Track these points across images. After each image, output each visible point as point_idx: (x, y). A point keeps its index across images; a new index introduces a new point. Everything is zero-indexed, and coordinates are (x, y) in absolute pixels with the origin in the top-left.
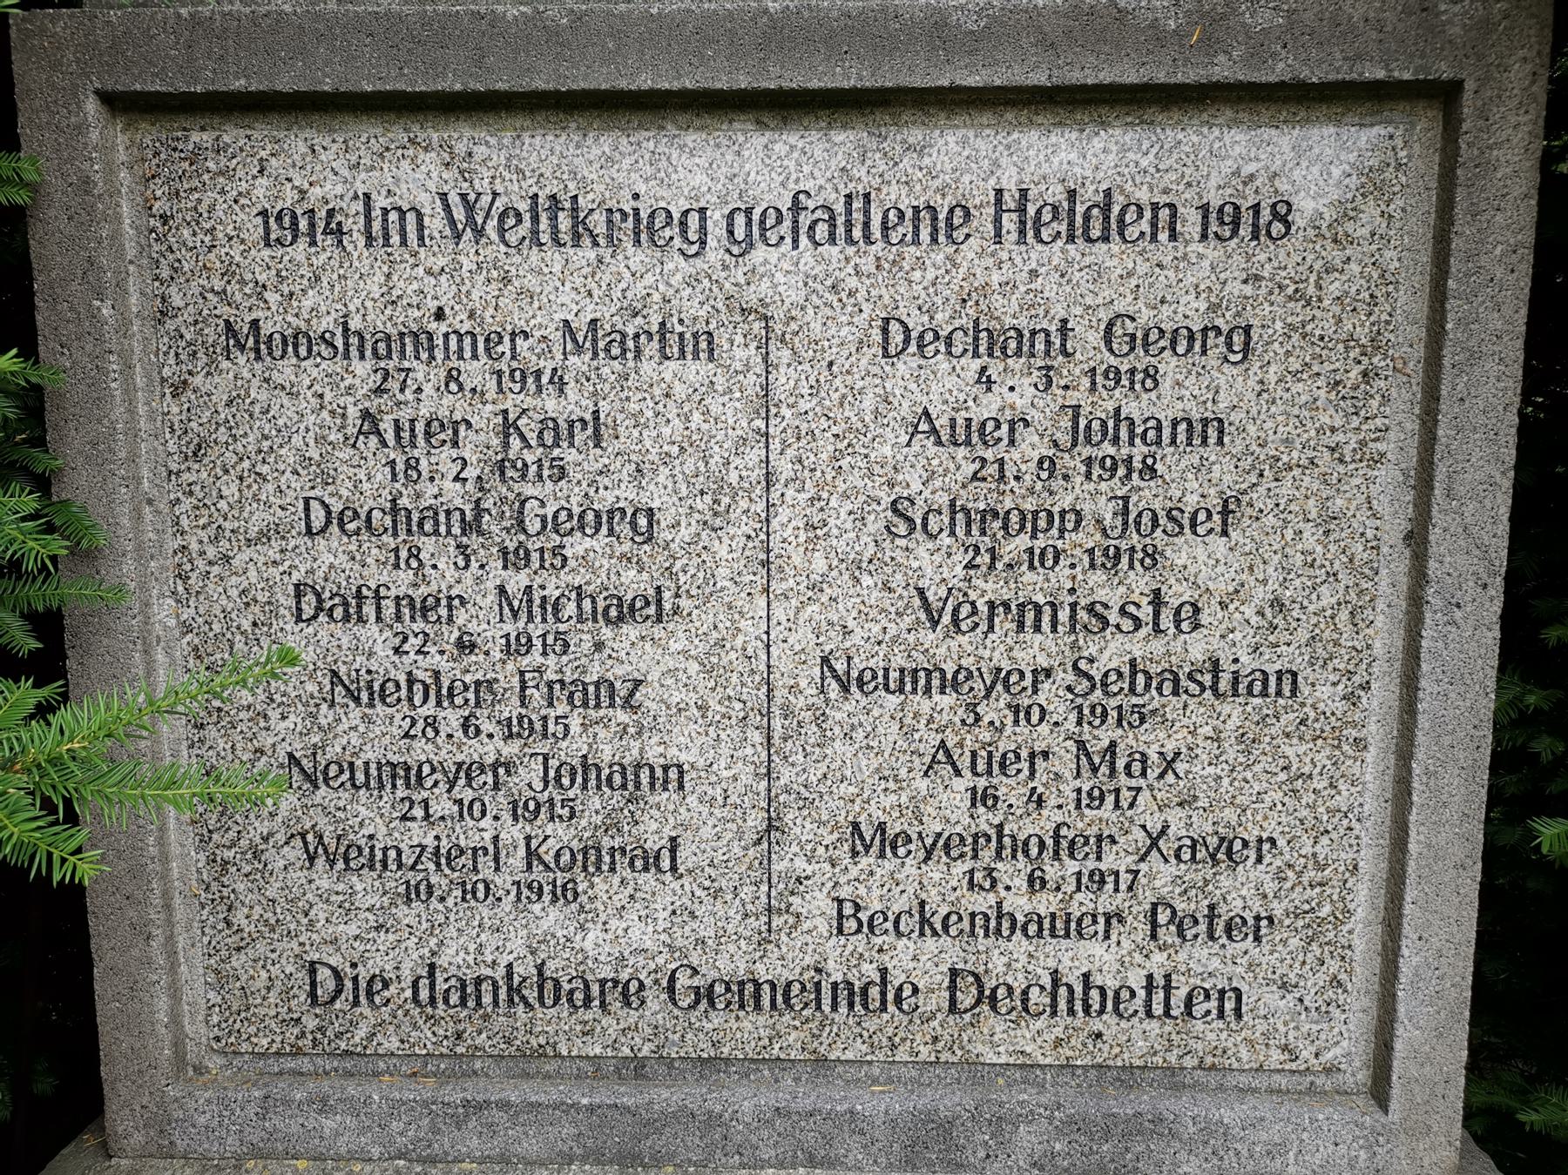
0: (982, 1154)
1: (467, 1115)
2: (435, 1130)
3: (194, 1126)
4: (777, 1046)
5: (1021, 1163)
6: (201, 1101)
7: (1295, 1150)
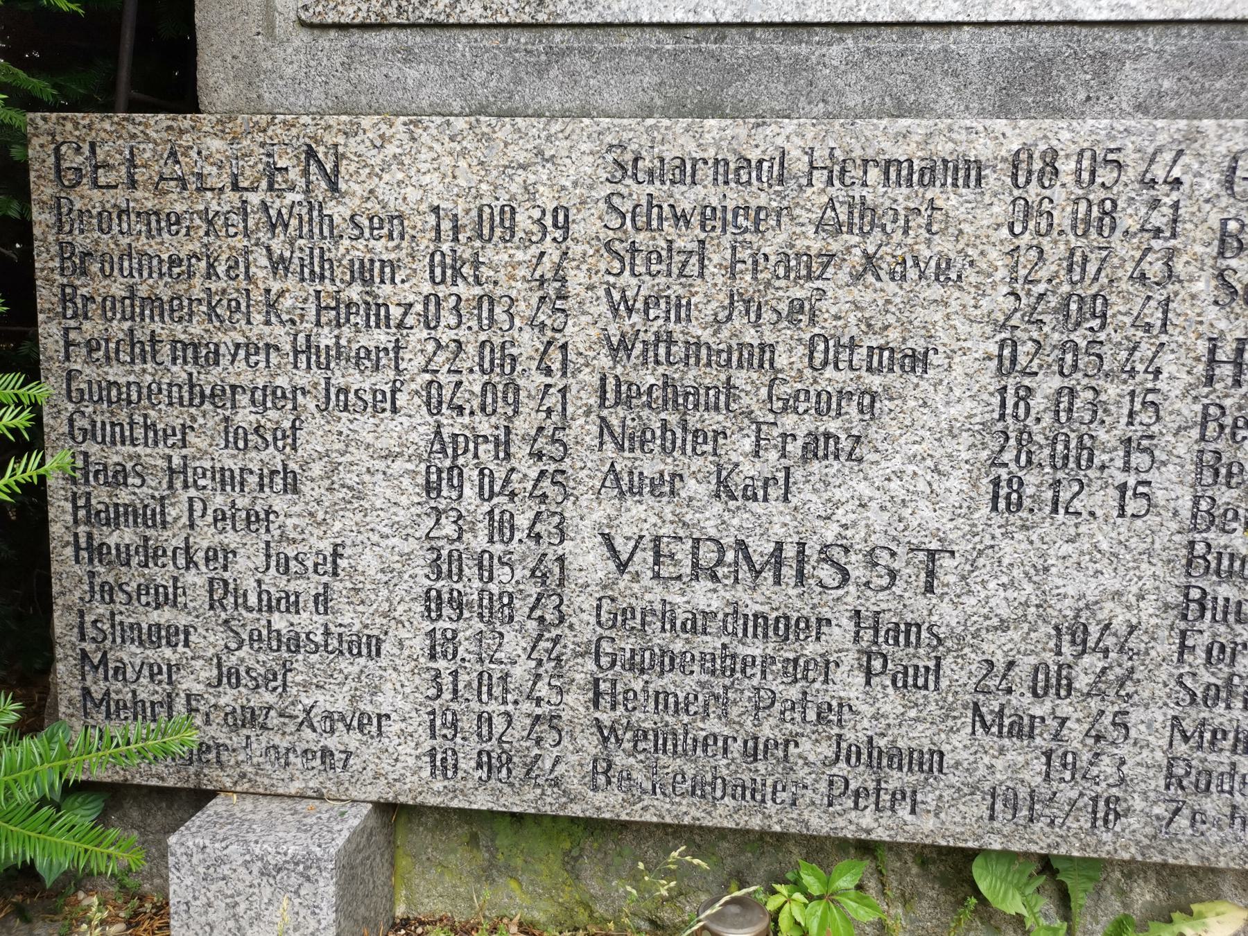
0: (1082, 96)
1: (549, 63)
2: (518, 81)
3: (281, 78)
5: (1124, 105)
6: (290, 50)
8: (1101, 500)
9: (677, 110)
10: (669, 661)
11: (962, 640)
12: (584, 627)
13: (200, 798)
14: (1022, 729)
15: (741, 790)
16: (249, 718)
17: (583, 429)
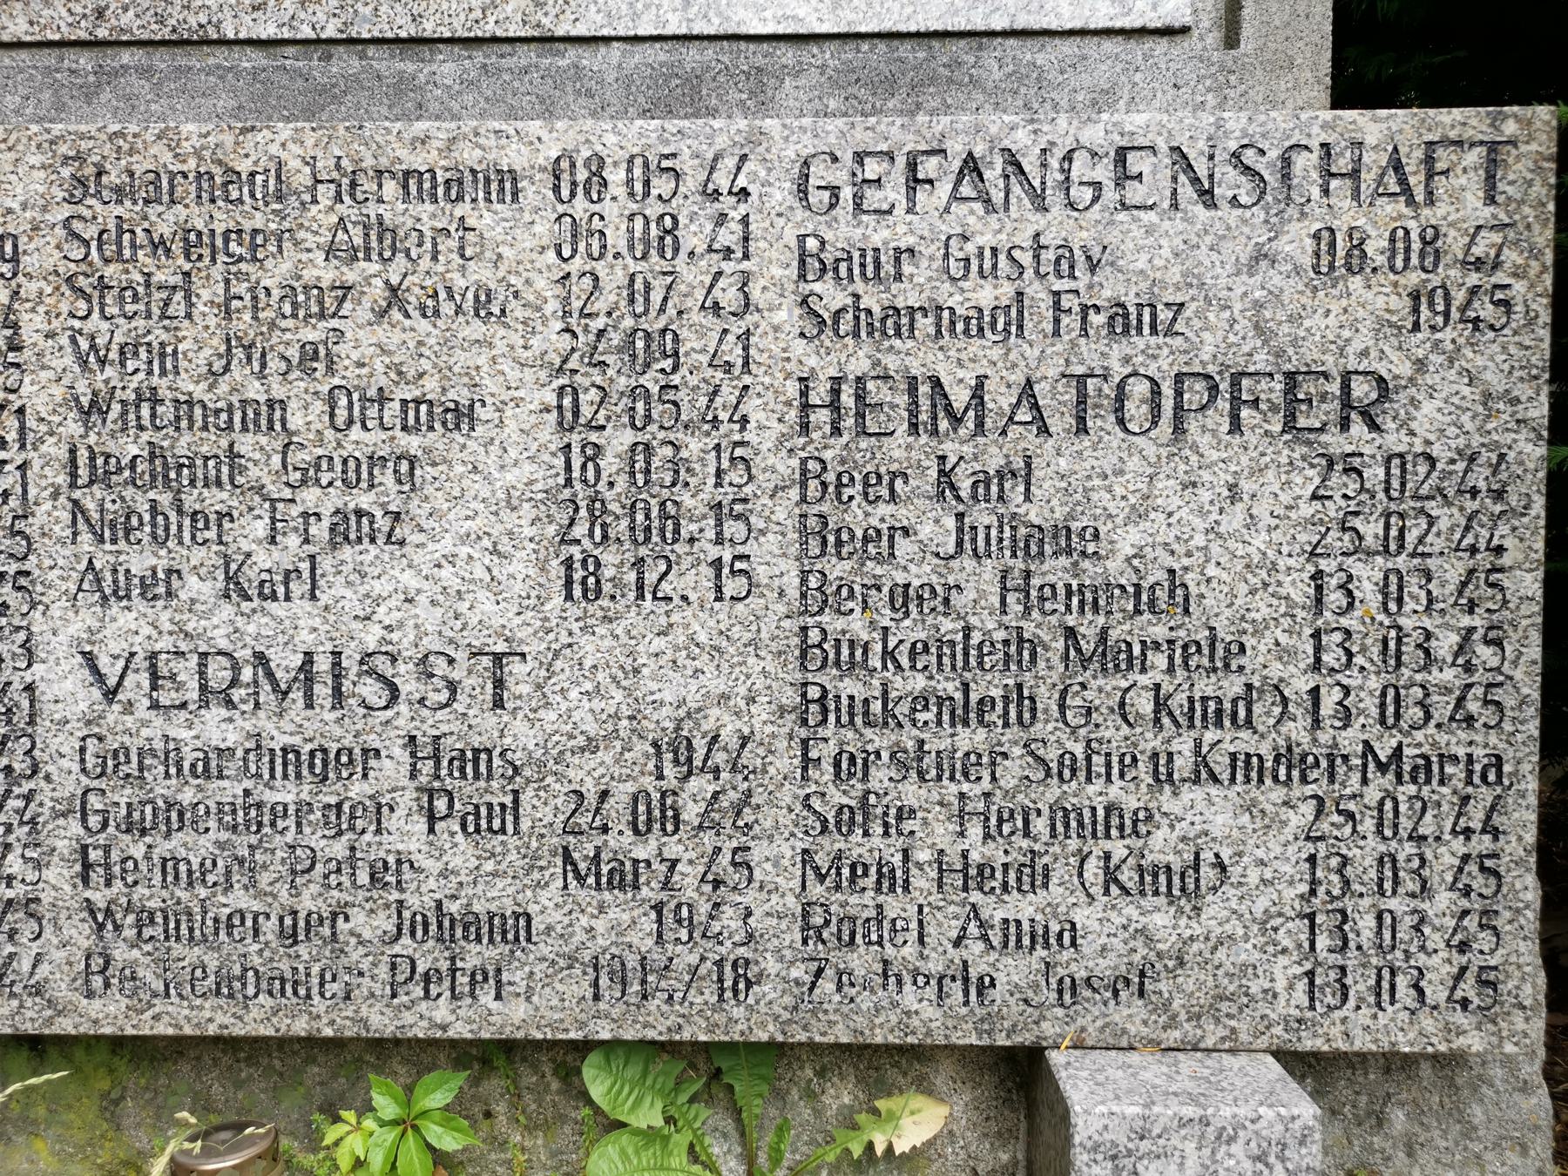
4: (491, 20)
7: (1126, 97)
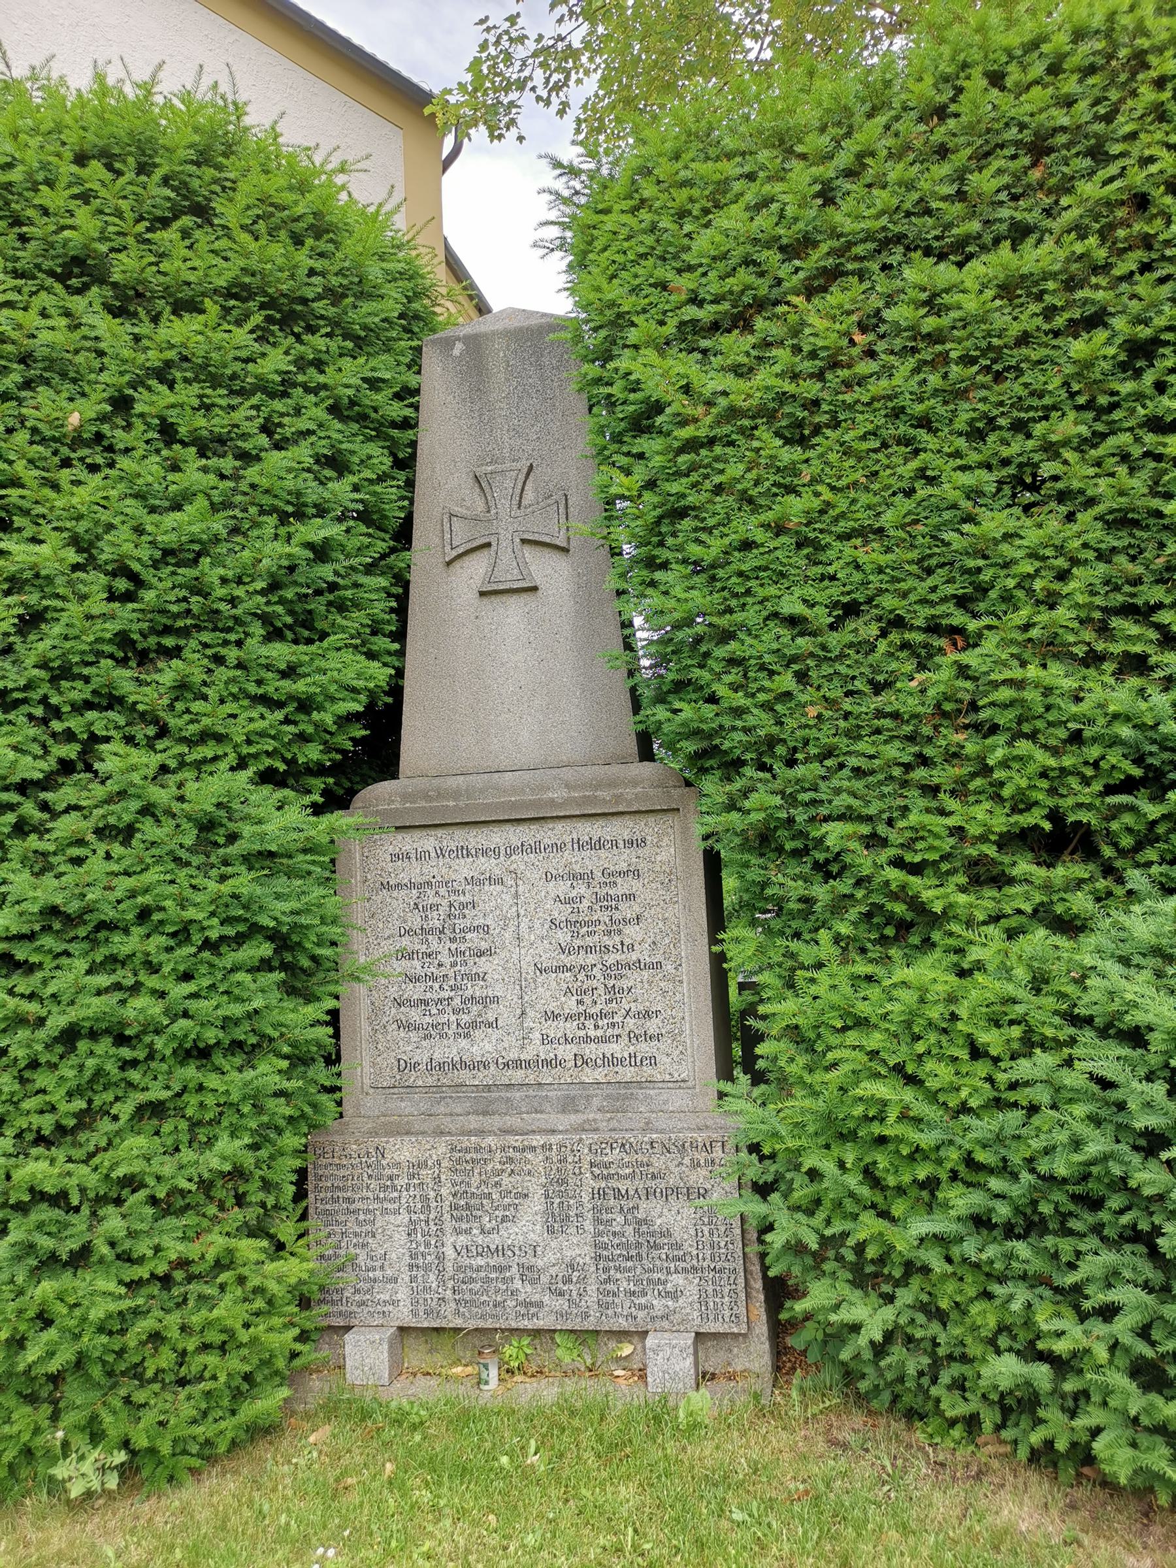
8: (573, 1230)
9: (476, 1113)
10: (472, 1280)
11: (544, 1270)
12: (450, 1271)
13: (348, 1328)
14: (561, 1294)
15: (493, 1316)
16: (363, 1303)
17: (447, 1216)
